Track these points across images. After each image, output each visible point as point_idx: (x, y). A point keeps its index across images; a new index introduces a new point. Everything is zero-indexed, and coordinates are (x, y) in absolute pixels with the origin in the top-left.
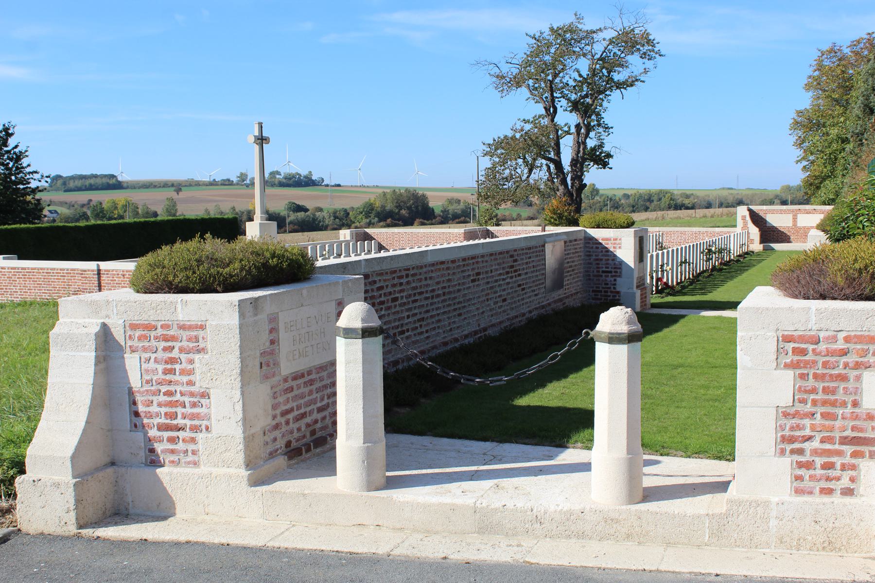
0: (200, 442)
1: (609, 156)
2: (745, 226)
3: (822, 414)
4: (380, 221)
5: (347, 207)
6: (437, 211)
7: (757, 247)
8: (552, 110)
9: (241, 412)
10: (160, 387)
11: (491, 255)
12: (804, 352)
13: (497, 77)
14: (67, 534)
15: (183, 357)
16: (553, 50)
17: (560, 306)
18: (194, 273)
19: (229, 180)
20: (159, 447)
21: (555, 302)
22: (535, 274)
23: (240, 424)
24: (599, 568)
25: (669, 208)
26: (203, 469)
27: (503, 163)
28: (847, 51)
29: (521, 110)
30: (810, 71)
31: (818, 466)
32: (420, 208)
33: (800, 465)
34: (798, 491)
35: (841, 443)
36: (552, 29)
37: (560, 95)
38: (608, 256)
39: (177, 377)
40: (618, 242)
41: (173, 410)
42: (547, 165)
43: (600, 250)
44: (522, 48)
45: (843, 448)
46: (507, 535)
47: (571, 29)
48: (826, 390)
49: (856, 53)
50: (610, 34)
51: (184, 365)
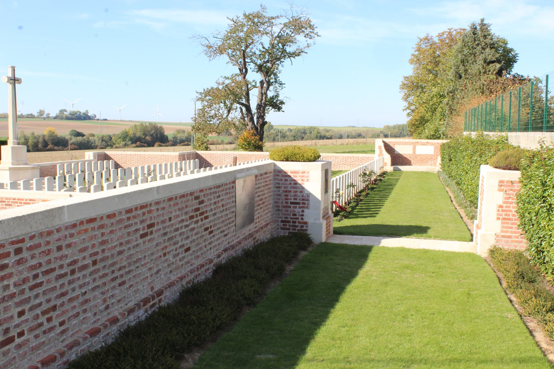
1: (282, 103)
2: (381, 154)
4: (132, 143)
5: (111, 133)
6: (170, 138)
7: (389, 168)
8: (244, 70)
11: (170, 199)
13: (207, 46)
16: (245, 29)
17: (249, 244)
19: (32, 115)
21: (245, 239)
22: (225, 213)
27: (210, 106)
28: (436, 40)
29: (224, 70)
32: (159, 135)
36: (245, 15)
37: (250, 61)
38: (296, 188)
40: (306, 175)
42: (240, 108)
43: (288, 182)
47: (258, 16)
50: (284, 20)
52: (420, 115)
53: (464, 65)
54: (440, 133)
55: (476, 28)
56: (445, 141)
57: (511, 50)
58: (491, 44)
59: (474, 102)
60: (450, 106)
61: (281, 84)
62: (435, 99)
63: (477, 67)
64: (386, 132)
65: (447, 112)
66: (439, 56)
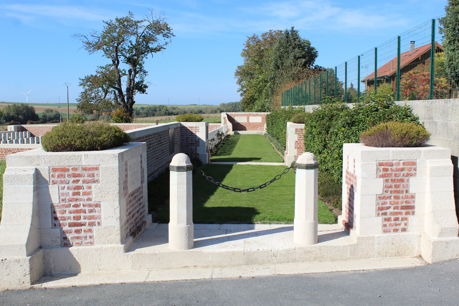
0: (95, 231)
1: (146, 87)
2: (225, 123)
3: (394, 197)
4: (6, 122)
6: (40, 116)
7: (231, 133)
8: (116, 62)
9: (119, 213)
10: (71, 203)
12: (386, 170)
13: (87, 43)
14: (24, 288)
15: (85, 185)
16: (117, 31)
18: (85, 140)
20: (69, 236)
23: (118, 219)
24: (313, 273)
25: (165, 114)
26: (96, 246)
28: (261, 38)
29: (99, 61)
30: (243, 47)
31: (392, 219)
32: (30, 115)
33: (386, 220)
34: (385, 231)
35: (401, 209)
36: (117, 20)
39: (81, 197)
40: (197, 129)
41: (79, 215)
44: (101, 29)
45: (402, 211)
46: (260, 264)
47: (127, 20)
48: (396, 186)
49: (265, 40)
50: (146, 24)
51: (85, 190)
52: (250, 95)
53: (280, 60)
54: (265, 107)
55: (288, 33)
56: (269, 113)
57: (313, 49)
58: (299, 45)
59: (289, 86)
60: (272, 89)
61: (145, 72)
62: (261, 83)
63: (289, 61)
64: (222, 109)
65: (270, 93)
66: (263, 50)
